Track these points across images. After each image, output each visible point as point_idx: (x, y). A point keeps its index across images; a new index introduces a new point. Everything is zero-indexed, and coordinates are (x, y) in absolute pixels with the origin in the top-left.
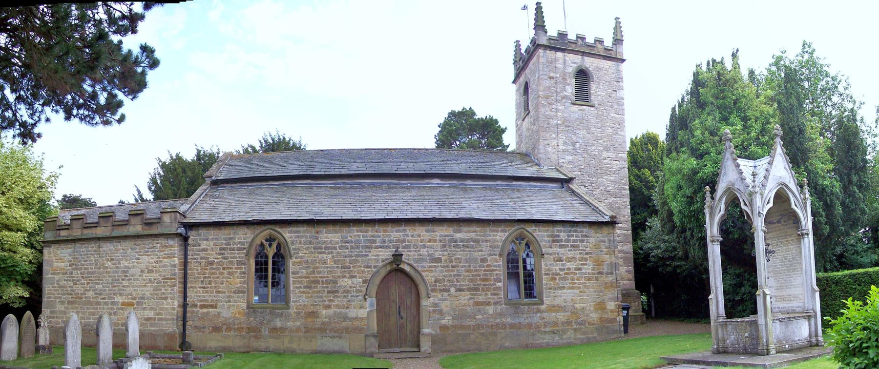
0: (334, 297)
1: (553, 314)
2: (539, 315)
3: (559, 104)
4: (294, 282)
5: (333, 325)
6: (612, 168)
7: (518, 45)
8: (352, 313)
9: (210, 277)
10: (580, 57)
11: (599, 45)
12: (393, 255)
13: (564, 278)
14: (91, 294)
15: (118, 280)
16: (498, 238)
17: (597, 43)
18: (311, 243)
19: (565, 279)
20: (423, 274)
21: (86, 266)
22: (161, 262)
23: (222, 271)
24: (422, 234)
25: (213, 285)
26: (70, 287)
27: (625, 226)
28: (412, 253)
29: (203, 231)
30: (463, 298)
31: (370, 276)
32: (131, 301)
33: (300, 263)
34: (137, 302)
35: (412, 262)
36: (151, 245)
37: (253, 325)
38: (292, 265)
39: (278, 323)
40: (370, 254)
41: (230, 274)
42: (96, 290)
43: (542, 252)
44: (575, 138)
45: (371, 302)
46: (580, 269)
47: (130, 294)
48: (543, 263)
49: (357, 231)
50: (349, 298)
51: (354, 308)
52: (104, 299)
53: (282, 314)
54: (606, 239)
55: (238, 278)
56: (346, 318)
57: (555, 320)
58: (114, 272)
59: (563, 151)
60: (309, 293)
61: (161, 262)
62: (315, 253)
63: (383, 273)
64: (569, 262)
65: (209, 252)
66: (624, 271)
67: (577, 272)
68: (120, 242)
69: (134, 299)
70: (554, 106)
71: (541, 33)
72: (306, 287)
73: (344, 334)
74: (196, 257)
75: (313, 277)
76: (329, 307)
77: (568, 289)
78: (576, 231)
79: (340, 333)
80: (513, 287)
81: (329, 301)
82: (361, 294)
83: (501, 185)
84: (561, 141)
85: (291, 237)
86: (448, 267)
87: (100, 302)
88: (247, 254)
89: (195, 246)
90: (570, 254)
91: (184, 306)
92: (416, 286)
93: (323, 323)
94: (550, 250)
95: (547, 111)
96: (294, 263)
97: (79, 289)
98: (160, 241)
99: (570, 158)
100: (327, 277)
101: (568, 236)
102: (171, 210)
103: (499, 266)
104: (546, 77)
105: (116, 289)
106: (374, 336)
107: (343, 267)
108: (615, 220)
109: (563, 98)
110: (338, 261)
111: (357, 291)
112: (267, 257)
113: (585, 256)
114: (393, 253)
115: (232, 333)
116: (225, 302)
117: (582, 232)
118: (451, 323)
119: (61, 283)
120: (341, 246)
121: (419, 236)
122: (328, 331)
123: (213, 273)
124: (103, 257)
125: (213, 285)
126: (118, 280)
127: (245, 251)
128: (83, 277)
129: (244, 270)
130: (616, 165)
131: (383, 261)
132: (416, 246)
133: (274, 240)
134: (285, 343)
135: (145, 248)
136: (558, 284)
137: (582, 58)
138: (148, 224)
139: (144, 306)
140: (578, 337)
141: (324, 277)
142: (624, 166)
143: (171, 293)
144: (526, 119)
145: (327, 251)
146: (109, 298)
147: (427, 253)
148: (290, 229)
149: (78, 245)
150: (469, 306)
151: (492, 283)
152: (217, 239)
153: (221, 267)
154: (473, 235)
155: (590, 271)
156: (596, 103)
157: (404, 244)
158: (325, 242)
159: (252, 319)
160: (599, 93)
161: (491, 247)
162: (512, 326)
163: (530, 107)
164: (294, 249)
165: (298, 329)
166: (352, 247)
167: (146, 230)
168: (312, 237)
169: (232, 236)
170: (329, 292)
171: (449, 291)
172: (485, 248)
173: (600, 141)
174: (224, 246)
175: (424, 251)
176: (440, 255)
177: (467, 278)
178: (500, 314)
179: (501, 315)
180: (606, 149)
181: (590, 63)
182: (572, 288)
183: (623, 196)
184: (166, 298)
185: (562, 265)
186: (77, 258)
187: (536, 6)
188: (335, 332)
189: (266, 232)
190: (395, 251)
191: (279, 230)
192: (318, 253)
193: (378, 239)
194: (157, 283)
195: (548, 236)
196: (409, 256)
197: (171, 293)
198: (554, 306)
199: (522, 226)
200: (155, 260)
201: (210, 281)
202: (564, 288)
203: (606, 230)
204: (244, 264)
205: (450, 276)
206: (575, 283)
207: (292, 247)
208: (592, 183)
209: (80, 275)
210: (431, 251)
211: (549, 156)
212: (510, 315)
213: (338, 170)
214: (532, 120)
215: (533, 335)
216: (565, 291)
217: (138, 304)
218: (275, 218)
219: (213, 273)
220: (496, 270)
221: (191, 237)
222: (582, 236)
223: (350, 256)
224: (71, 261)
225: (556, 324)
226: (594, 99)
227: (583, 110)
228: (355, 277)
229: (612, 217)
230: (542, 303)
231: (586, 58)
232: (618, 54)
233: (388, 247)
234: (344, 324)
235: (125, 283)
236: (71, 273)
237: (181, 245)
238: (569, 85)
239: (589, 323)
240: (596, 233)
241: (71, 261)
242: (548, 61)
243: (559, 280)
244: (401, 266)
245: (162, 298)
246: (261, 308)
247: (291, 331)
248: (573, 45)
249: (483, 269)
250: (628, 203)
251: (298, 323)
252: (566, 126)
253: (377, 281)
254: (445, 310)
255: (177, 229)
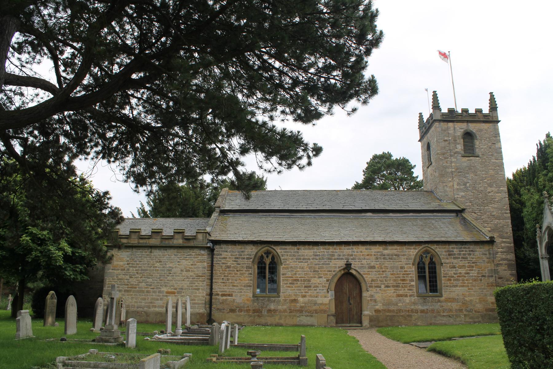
0: (308, 290)
1: (449, 304)
2: (439, 304)
3: (452, 158)
4: (283, 280)
5: (307, 308)
6: (496, 198)
7: (421, 116)
8: (320, 300)
9: (228, 276)
10: (465, 124)
11: (478, 114)
12: (345, 264)
13: (457, 279)
14: (143, 284)
15: (164, 276)
16: (412, 253)
17: (478, 112)
18: (294, 255)
19: (457, 280)
20: (364, 276)
21: (140, 265)
22: (195, 265)
23: (236, 272)
24: (363, 251)
25: (230, 281)
26: (126, 279)
27: (509, 240)
28: (357, 263)
29: (224, 246)
30: (390, 292)
31: (331, 277)
32: (173, 290)
33: (287, 268)
34: (178, 291)
35: (357, 269)
36: (189, 254)
37: (257, 308)
38: (282, 270)
39: (272, 307)
40: (331, 263)
41: (242, 274)
42: (147, 282)
43: (441, 261)
44: (465, 180)
45: (332, 294)
46: (468, 273)
47: (172, 286)
48: (442, 270)
49: (323, 249)
50: (318, 291)
51: (321, 297)
52: (153, 288)
53: (275, 301)
54: (487, 253)
55: (247, 277)
56: (315, 304)
57: (451, 308)
58: (161, 270)
59: (457, 189)
60: (292, 287)
61: (195, 265)
62: (297, 262)
63: (339, 275)
64: (460, 268)
65: (228, 259)
66: (508, 274)
67: (466, 275)
68: (166, 250)
69: (175, 289)
70: (448, 159)
71: (437, 111)
72: (290, 283)
73: (314, 314)
74: (219, 262)
75: (295, 277)
76: (305, 296)
77: (459, 287)
78: (465, 248)
79: (311, 313)
80: (422, 286)
81: (306, 292)
82: (325, 288)
83: (413, 216)
84: (455, 183)
85: (281, 252)
86: (379, 271)
87: (150, 291)
88: (253, 262)
89: (219, 255)
90: (461, 264)
91: (211, 294)
92: (359, 284)
93: (301, 307)
94: (447, 261)
95: (444, 163)
96: (284, 268)
97: (133, 281)
98: (195, 251)
99: (463, 194)
100: (304, 277)
101: (460, 251)
102: (203, 231)
103: (412, 271)
104: (442, 140)
105: (163, 282)
106: (333, 316)
107: (314, 271)
108: (493, 239)
109: (455, 153)
110: (311, 267)
111: (323, 286)
112: (265, 264)
113: (472, 264)
114: (346, 263)
115: (243, 313)
116: (238, 292)
117: (469, 248)
118: (382, 308)
119: (120, 277)
120: (313, 258)
121: (361, 252)
122: (304, 312)
123: (230, 274)
124: (153, 259)
125: (230, 281)
126: (164, 276)
127: (251, 260)
128: (137, 273)
129: (250, 272)
130: (498, 196)
131: (339, 268)
132: (359, 259)
133: (270, 253)
134: (276, 320)
135: (184, 255)
136: (453, 283)
137: (467, 125)
138: (187, 239)
139: (183, 294)
140: (467, 320)
141: (302, 277)
142: (504, 196)
143: (202, 286)
144: (430, 167)
145: (304, 261)
146: (157, 288)
147: (366, 263)
148: (281, 247)
149: (134, 250)
150: (393, 297)
151: (408, 282)
152: (233, 252)
153: (236, 270)
154: (395, 252)
155: (476, 275)
156: (480, 154)
157: (352, 257)
158: (303, 255)
159: (256, 304)
160: (482, 147)
161: (407, 259)
162: (422, 311)
163: (432, 160)
164: (283, 259)
165: (285, 311)
166: (320, 259)
167: (185, 243)
168: (295, 252)
169: (243, 250)
170: (305, 287)
171: (380, 287)
172: (403, 260)
173: (485, 180)
174: (238, 256)
175: (364, 262)
176: (374, 264)
177: (392, 279)
178: (414, 303)
179: (414, 303)
180: (490, 185)
181: (473, 127)
182: (463, 286)
183: (506, 218)
184: (198, 289)
185: (456, 270)
186: (133, 259)
187: (433, 94)
188: (308, 312)
189: (266, 248)
190: (347, 262)
191: (274, 247)
192: (299, 262)
193: (336, 254)
194: (192, 279)
195: (445, 252)
196: (355, 265)
197: (202, 286)
198: (450, 299)
199: (427, 245)
200: (191, 263)
201: (228, 279)
202: (457, 286)
203: (487, 247)
204: (251, 268)
205: (381, 277)
206: (465, 283)
207: (282, 258)
208: (480, 210)
209: (135, 272)
210: (369, 262)
211: (447, 194)
212: (420, 304)
213: (304, 206)
214: (434, 168)
215: (435, 317)
216: (458, 288)
217: (178, 293)
218: (271, 240)
219: (230, 274)
220: (410, 274)
221: (216, 250)
222: (469, 251)
223: (319, 264)
224: (128, 261)
225: (451, 310)
226: (478, 151)
227: (471, 160)
228: (321, 277)
229: (491, 238)
230: (441, 296)
231: (470, 124)
232: (494, 118)
233: (342, 259)
234: (314, 308)
235: (170, 278)
236: (128, 270)
237: (209, 254)
238: (459, 144)
239: (475, 311)
240: (480, 248)
241: (128, 261)
242: (442, 130)
243: (454, 280)
244: (350, 271)
245: (195, 289)
246: (262, 297)
247: (280, 312)
248: (460, 117)
249: (402, 273)
250: (510, 223)
251: (285, 307)
252: (459, 172)
253: (336, 280)
254: (378, 299)
255: (207, 244)
